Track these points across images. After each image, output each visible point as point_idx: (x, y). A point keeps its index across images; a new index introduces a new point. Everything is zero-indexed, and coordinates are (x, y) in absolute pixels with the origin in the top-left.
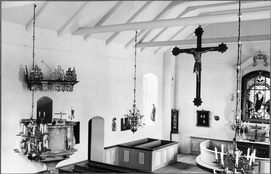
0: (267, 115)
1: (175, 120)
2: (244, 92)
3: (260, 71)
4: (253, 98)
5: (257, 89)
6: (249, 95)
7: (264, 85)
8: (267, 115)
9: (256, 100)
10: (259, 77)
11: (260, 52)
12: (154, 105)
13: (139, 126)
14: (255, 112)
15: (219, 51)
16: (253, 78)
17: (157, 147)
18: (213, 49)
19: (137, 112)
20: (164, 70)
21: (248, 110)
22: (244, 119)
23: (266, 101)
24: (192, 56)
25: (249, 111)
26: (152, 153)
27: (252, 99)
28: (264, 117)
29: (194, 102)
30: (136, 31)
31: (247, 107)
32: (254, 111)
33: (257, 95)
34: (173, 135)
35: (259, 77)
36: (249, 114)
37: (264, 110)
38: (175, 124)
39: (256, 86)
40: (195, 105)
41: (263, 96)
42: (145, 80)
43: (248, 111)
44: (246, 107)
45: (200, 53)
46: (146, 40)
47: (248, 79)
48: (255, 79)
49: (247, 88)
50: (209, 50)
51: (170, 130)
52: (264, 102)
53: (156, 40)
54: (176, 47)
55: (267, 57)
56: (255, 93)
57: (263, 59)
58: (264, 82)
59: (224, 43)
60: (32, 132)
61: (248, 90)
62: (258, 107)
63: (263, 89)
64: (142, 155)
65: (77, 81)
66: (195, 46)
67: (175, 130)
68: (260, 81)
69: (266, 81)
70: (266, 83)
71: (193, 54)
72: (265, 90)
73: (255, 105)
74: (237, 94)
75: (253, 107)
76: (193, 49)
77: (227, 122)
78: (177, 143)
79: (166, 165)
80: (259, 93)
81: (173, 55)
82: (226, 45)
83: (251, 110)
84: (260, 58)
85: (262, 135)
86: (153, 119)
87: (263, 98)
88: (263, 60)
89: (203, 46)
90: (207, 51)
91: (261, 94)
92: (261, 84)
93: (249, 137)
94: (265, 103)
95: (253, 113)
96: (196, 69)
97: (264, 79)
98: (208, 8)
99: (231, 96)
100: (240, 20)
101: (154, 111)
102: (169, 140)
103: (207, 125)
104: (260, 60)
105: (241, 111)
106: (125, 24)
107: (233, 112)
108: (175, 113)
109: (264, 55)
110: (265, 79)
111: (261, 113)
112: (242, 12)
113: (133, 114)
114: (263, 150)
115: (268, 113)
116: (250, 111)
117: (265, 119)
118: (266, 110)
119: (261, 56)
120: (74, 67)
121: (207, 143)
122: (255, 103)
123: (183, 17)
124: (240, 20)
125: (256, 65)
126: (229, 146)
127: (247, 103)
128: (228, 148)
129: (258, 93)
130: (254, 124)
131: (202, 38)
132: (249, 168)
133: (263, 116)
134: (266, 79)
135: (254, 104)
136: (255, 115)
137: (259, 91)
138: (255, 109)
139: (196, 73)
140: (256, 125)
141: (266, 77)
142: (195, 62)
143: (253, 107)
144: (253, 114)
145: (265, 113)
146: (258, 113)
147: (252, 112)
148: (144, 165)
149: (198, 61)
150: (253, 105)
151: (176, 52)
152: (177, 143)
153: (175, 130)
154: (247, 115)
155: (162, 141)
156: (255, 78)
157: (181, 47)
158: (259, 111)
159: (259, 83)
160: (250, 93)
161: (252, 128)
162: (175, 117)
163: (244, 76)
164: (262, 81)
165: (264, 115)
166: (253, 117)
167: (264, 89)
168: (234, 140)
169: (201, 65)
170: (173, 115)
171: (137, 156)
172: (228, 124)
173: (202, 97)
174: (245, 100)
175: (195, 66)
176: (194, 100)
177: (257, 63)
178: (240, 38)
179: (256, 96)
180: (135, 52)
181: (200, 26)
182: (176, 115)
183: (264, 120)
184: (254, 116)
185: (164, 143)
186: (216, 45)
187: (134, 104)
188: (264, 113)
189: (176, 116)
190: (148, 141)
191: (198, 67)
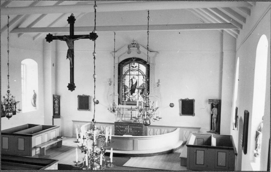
1: (56, 105)
2: (120, 77)
3: (134, 58)
4: (129, 83)
6: (125, 80)
7: (137, 71)
9: (131, 84)
10: (133, 64)
11: (134, 41)
12: (34, 90)
14: (131, 95)
15: (90, 39)
16: (128, 64)
17: (37, 132)
18: (85, 37)
19: (11, 97)
23: (140, 85)
25: (125, 94)
26: (31, 139)
27: (127, 83)
29: (68, 87)
30: (8, 16)
31: (123, 91)
32: (129, 95)
33: (132, 79)
34: (54, 119)
35: (133, 64)
36: (125, 98)
37: (138, 94)
38: (57, 109)
40: (69, 90)
41: (137, 81)
42: (25, 66)
44: (123, 91)
45: (72, 40)
46: (25, 25)
48: (130, 66)
49: (123, 73)
51: (52, 115)
53: (35, 26)
54: (49, 34)
55: (139, 45)
57: (137, 47)
58: (137, 68)
61: (124, 75)
62: (132, 91)
63: (136, 74)
64: (21, 141)
66: (68, 33)
67: (57, 114)
69: (139, 67)
71: (66, 40)
72: (139, 75)
73: (130, 89)
74: (94, 79)
75: (128, 91)
76: (65, 36)
78: (59, 127)
79: (47, 149)
81: (47, 41)
84: (134, 47)
86: (34, 105)
87: (136, 82)
88: (136, 48)
89: (76, 33)
90: (79, 38)
91: (135, 79)
94: (139, 87)
95: (129, 96)
96: (69, 56)
97: (137, 65)
99: (108, 81)
100: (95, 11)
101: (35, 97)
102: (51, 125)
105: (118, 95)
107: (111, 96)
108: (57, 99)
109: (137, 44)
110: (138, 65)
111: (135, 96)
112: (97, 4)
113: (8, 100)
114: (137, 129)
119: (134, 44)
121: (88, 125)
122: (130, 88)
123: (60, 4)
124: (95, 11)
125: (130, 53)
127: (123, 87)
129: (132, 78)
132: (105, 145)
134: (139, 65)
135: (129, 88)
136: (130, 98)
139: (69, 59)
140: (131, 107)
141: (139, 63)
142: (68, 48)
143: (128, 91)
144: (128, 97)
147: (127, 95)
148: (204, 165)
149: (71, 48)
150: (129, 89)
151: (50, 38)
152: (59, 127)
153: (57, 114)
155: (43, 126)
156: (130, 65)
157: (53, 34)
158: (134, 94)
159: (133, 68)
160: (126, 78)
162: (56, 102)
163: (121, 63)
164: (136, 67)
165: (138, 98)
166: (129, 100)
168: (93, 121)
169: (74, 52)
170: (55, 101)
171: (17, 143)
174: (121, 84)
175: (68, 53)
176: (68, 85)
177: (131, 50)
178: (96, 27)
180: (7, 37)
181: (72, 15)
182: (57, 100)
184: (130, 99)
185: (45, 128)
186: (88, 33)
187: (8, 90)
188: (138, 96)
189: (58, 101)
190: (29, 127)
191: (71, 54)
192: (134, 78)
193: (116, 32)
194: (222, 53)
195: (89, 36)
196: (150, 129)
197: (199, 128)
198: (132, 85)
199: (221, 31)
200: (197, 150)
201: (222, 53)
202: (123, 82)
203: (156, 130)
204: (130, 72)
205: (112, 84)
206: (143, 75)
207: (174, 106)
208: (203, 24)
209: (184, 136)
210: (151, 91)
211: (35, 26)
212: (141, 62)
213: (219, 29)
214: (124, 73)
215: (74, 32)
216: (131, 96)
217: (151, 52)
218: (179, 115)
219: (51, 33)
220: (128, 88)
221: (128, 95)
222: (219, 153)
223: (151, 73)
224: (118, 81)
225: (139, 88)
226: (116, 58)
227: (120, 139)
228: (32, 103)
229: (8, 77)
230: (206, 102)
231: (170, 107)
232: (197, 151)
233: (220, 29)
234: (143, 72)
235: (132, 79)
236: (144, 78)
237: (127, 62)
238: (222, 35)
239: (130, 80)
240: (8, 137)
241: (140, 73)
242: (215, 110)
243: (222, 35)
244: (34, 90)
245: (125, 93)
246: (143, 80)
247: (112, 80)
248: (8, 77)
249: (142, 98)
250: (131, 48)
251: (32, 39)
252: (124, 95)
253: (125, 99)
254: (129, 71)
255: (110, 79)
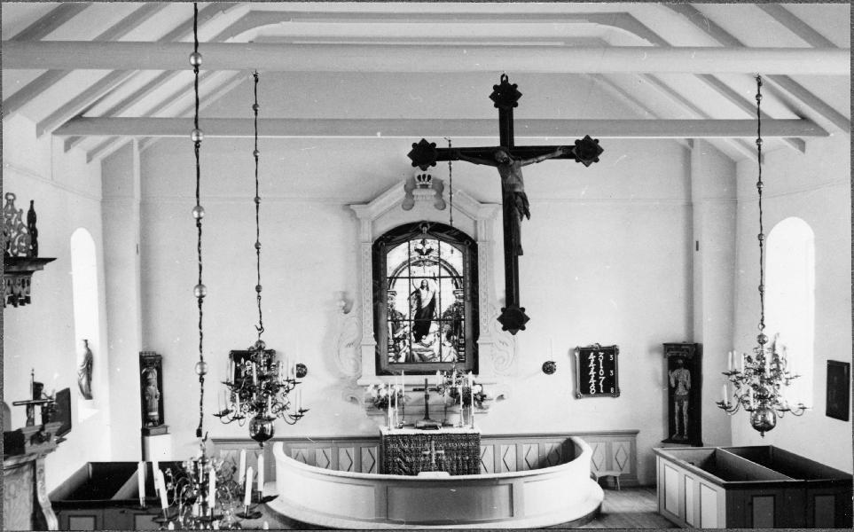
0: (449, 349)
3: (424, 224)
5: (416, 275)
7: (435, 263)
8: (449, 349)
9: (415, 307)
10: (420, 241)
12: (86, 341)
13: (783, 410)
14: (416, 342)
15: (577, 161)
20: (105, 217)
21: (394, 339)
22: (384, 366)
23: (444, 310)
24: (493, 171)
25: (397, 340)
28: (440, 355)
33: (417, 292)
36: (397, 351)
39: (412, 267)
43: (395, 342)
47: (390, 247)
50: (549, 155)
52: (438, 313)
54: (423, 140)
56: (412, 287)
59: (593, 138)
60: (204, 496)
61: (391, 278)
62: (421, 329)
63: (432, 276)
65: (41, 255)
66: (494, 140)
68: (425, 251)
69: (439, 252)
70: (442, 257)
72: (440, 277)
73: (413, 322)
75: (407, 329)
77: (332, 380)
80: (422, 287)
82: (597, 141)
83: (401, 339)
84: (424, 187)
85: (446, 408)
87: (433, 300)
89: (520, 140)
90: (544, 157)
91: (428, 289)
92: (426, 260)
93: (406, 417)
95: (410, 347)
98: (519, 25)
99: (340, 300)
103: (610, 386)
104: (424, 192)
106: (95, 43)
115: (450, 344)
116: (399, 342)
117: (443, 360)
118: (444, 336)
120: (32, 202)
122: (413, 318)
123: (230, 40)
126: (342, 452)
127: (389, 318)
128: (341, 458)
129: (418, 286)
130: (418, 380)
131: (514, 118)
133: (437, 352)
135: (410, 320)
137: (422, 282)
138: (415, 335)
140: (426, 380)
144: (408, 350)
145: (441, 344)
146: (423, 345)
147: (405, 344)
150: (408, 323)
154: (393, 354)
158: (427, 340)
159: (422, 257)
161: (415, 390)
162: (153, 377)
164: (430, 251)
165: (440, 351)
166: (410, 360)
167: (436, 275)
172: (336, 386)
173: (523, 302)
177: (415, 199)
179: (414, 295)
181: (504, 79)
183: (443, 365)
184: (413, 355)
186: (569, 141)
188: (441, 344)
192: (425, 289)
193: (451, 138)
194: (690, 206)
195: (574, 151)
196: (506, 447)
197: (635, 433)
198: (419, 309)
199: (687, 144)
200: (752, 496)
201: (690, 206)
202: (389, 302)
203: (503, 448)
204: (412, 267)
205: (353, 311)
206: (454, 278)
207: (305, 373)
208: (655, 121)
209: (524, 461)
210: (485, 329)
211: (85, 116)
212: (448, 237)
213: (682, 138)
214: (390, 273)
215: (515, 137)
216: (415, 346)
217: (482, 203)
218: (571, 397)
219: (430, 139)
220: (404, 320)
221: (407, 341)
222: (72, 519)
223: (484, 270)
224: (375, 300)
225: (444, 320)
226: (367, 226)
227: (471, 485)
228: (81, 387)
229: (259, 291)
230: (652, 350)
231: (543, 373)
232: (755, 499)
233: (683, 137)
234: (454, 266)
235: (417, 292)
236: (457, 287)
237: (400, 237)
238: (687, 153)
239: (411, 295)
240: (774, 495)
241: (442, 270)
242: (684, 375)
243: (687, 153)
244: (86, 341)
245: (396, 336)
246: (454, 292)
247: (352, 296)
248: (259, 291)
249: (453, 349)
250: (415, 193)
251: (85, 159)
252: (392, 343)
253: (398, 357)
254: (408, 264)
255: (344, 293)
